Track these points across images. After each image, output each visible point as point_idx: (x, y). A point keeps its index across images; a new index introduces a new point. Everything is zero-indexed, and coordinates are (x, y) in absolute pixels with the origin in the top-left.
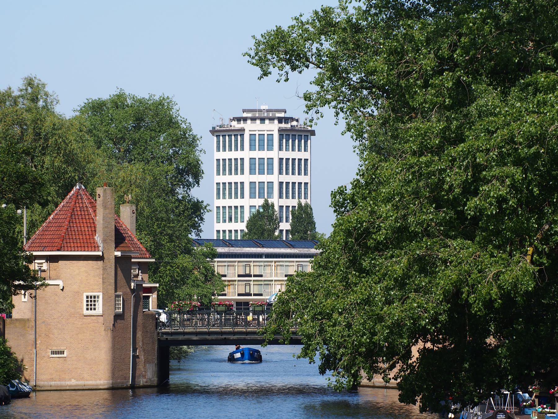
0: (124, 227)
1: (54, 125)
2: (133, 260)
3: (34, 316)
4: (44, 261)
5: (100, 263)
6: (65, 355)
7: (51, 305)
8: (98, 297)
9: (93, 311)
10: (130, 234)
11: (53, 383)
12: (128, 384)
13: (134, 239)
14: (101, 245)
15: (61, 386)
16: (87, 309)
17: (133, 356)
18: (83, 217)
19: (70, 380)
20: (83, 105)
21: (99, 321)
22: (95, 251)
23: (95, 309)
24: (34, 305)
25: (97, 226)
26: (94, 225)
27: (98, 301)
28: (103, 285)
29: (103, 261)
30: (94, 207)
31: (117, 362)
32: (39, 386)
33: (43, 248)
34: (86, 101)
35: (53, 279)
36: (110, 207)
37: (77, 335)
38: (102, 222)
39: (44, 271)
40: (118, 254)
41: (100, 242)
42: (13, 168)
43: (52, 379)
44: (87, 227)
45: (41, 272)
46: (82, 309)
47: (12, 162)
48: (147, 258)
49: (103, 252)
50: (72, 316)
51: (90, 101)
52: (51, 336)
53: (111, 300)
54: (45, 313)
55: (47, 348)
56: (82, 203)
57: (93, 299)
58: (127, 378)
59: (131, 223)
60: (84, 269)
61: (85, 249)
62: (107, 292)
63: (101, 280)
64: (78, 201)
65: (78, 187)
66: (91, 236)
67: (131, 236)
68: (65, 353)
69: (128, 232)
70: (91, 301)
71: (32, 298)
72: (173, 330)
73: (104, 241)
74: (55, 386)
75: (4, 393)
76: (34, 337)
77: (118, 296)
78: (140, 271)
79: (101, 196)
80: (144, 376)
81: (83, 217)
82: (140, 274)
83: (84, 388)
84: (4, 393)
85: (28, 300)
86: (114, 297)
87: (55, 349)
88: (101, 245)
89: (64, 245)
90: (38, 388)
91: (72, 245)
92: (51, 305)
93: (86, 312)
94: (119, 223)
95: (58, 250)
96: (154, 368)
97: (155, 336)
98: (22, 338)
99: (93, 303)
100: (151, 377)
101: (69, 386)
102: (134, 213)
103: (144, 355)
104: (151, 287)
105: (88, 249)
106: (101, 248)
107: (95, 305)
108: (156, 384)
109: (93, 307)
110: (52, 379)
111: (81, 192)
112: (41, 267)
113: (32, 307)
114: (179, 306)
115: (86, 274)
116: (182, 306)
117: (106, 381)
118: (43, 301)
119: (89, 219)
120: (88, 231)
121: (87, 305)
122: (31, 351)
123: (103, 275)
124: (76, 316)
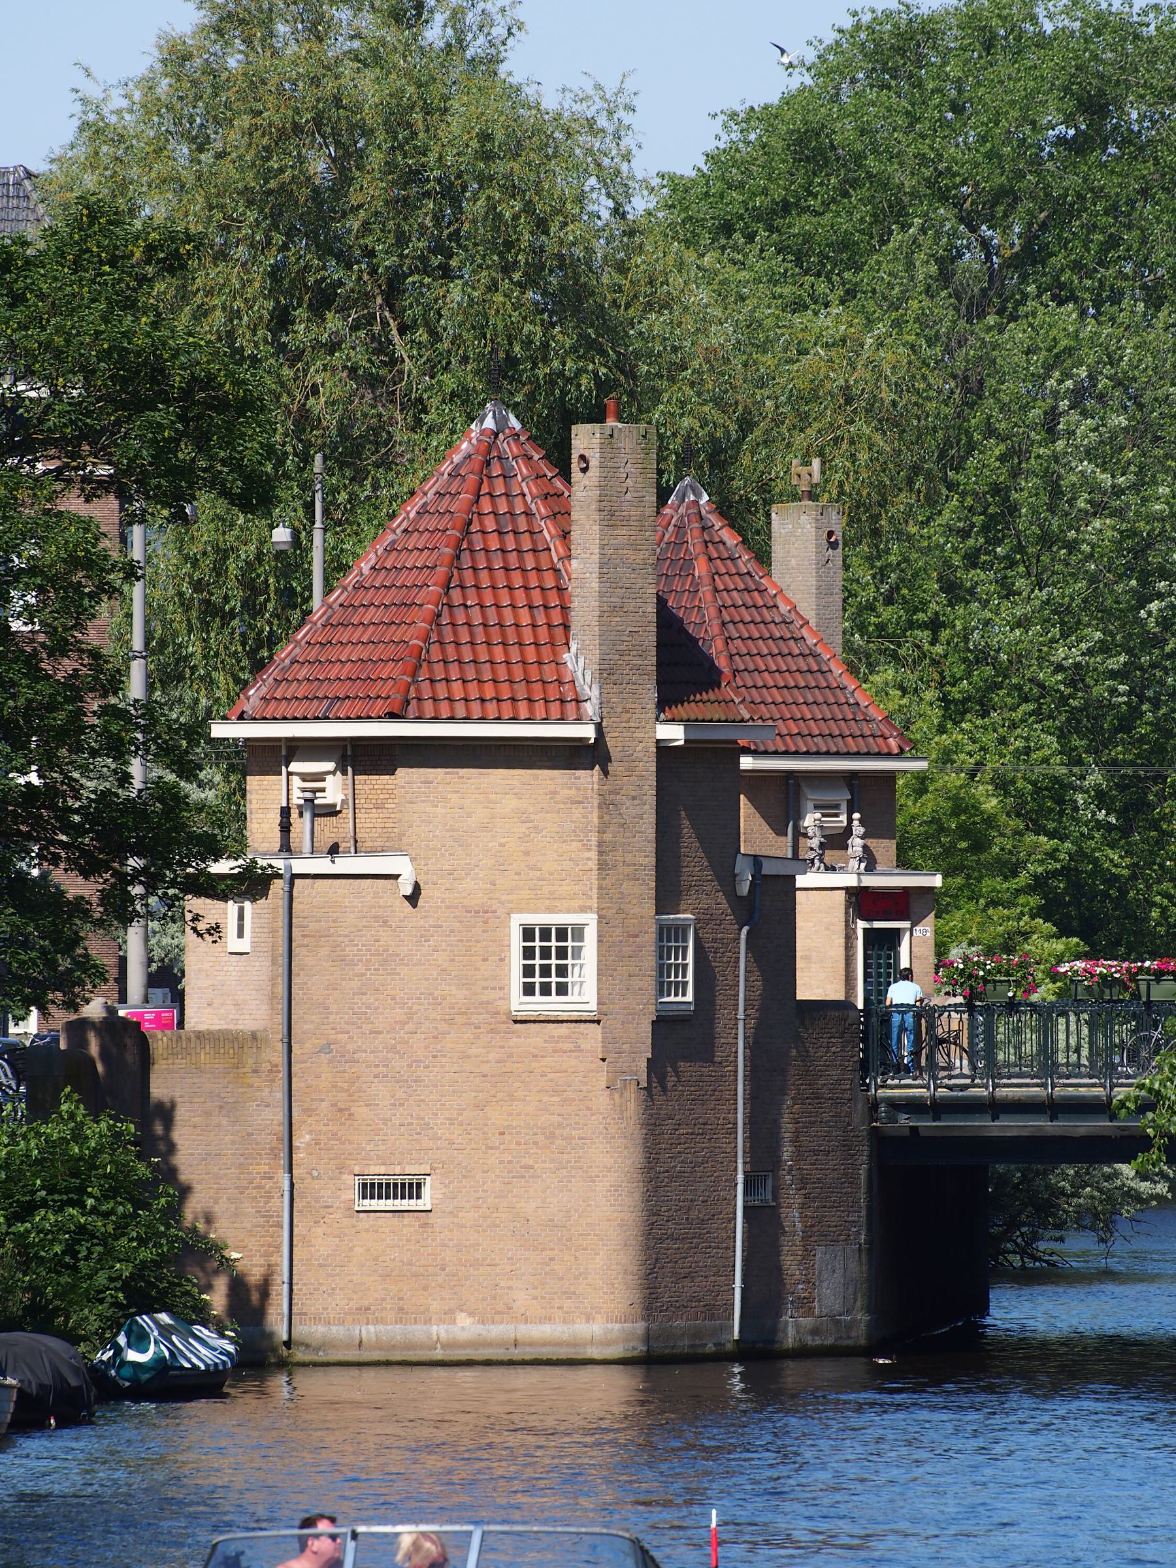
0: (784, 608)
1: (485, 137)
2: (747, 763)
3: (281, 1019)
4: (330, 766)
5: (588, 779)
6: (425, 1203)
7: (360, 969)
8: (579, 933)
9: (554, 998)
10: (810, 641)
11: (368, 1332)
12: (724, 1337)
13: (833, 665)
14: (591, 692)
15: (410, 1346)
16: (528, 990)
17: (745, 1208)
18: (513, 559)
19: (449, 1316)
20: (830, 37)
21: (586, 1045)
22: (562, 719)
23: (562, 990)
24: (282, 970)
25: (575, 604)
26: (561, 597)
27: (577, 952)
28: (601, 878)
29: (606, 773)
30: (561, 514)
31: (671, 1237)
32: (307, 1346)
33: (326, 703)
34: (848, 23)
35: (373, 852)
36: (635, 514)
37: (480, 1107)
38: (595, 585)
39: (331, 811)
40: (673, 733)
41: (588, 678)
42: (97, 333)
43: (364, 1312)
44: (531, 607)
45: (315, 815)
46: (504, 988)
47: (94, 300)
48: (889, 755)
49: (599, 727)
50: (459, 1019)
51: (866, 18)
52: (360, 1111)
53: (640, 948)
54: (334, 1008)
55: (341, 1169)
56: (507, 495)
57: (554, 943)
58: (719, 1311)
59: (822, 593)
60: (510, 804)
61: (515, 710)
62: (620, 911)
63: (593, 855)
64: (491, 486)
65: (489, 423)
66: (546, 651)
67: (819, 649)
68: (426, 1191)
69: (805, 632)
70: (546, 953)
71: (200, 935)
72: (942, 1092)
73: (607, 673)
74: (379, 1345)
75: (57, 1373)
76: (280, 1115)
77: (679, 931)
78: (856, 816)
79: (594, 463)
80: (805, 1305)
81: (513, 559)
82: (858, 829)
83: (517, 1354)
84: (57, 1373)
85: (254, 945)
86: (651, 936)
87: (377, 1170)
88: (591, 692)
89: (418, 690)
90: (300, 1355)
91: (457, 689)
92: (360, 969)
93: (519, 1003)
94: (762, 591)
95: (393, 716)
96: (853, 1266)
97: (856, 1118)
98: (224, 1121)
99: (554, 961)
100: (837, 1307)
101: (444, 1347)
102: (833, 546)
103: (803, 1206)
104: (906, 890)
105: (531, 710)
106: (589, 709)
107: (562, 971)
108: (862, 1342)
109: (554, 979)
110: (364, 1312)
111: (507, 447)
112: (314, 791)
113: (273, 979)
114: (970, 976)
115: (523, 829)
116: (986, 981)
117: (617, 1326)
118: (324, 952)
119: (538, 569)
120: (534, 626)
121: (528, 971)
122: (269, 1185)
123: (601, 831)
124: (475, 1019)
